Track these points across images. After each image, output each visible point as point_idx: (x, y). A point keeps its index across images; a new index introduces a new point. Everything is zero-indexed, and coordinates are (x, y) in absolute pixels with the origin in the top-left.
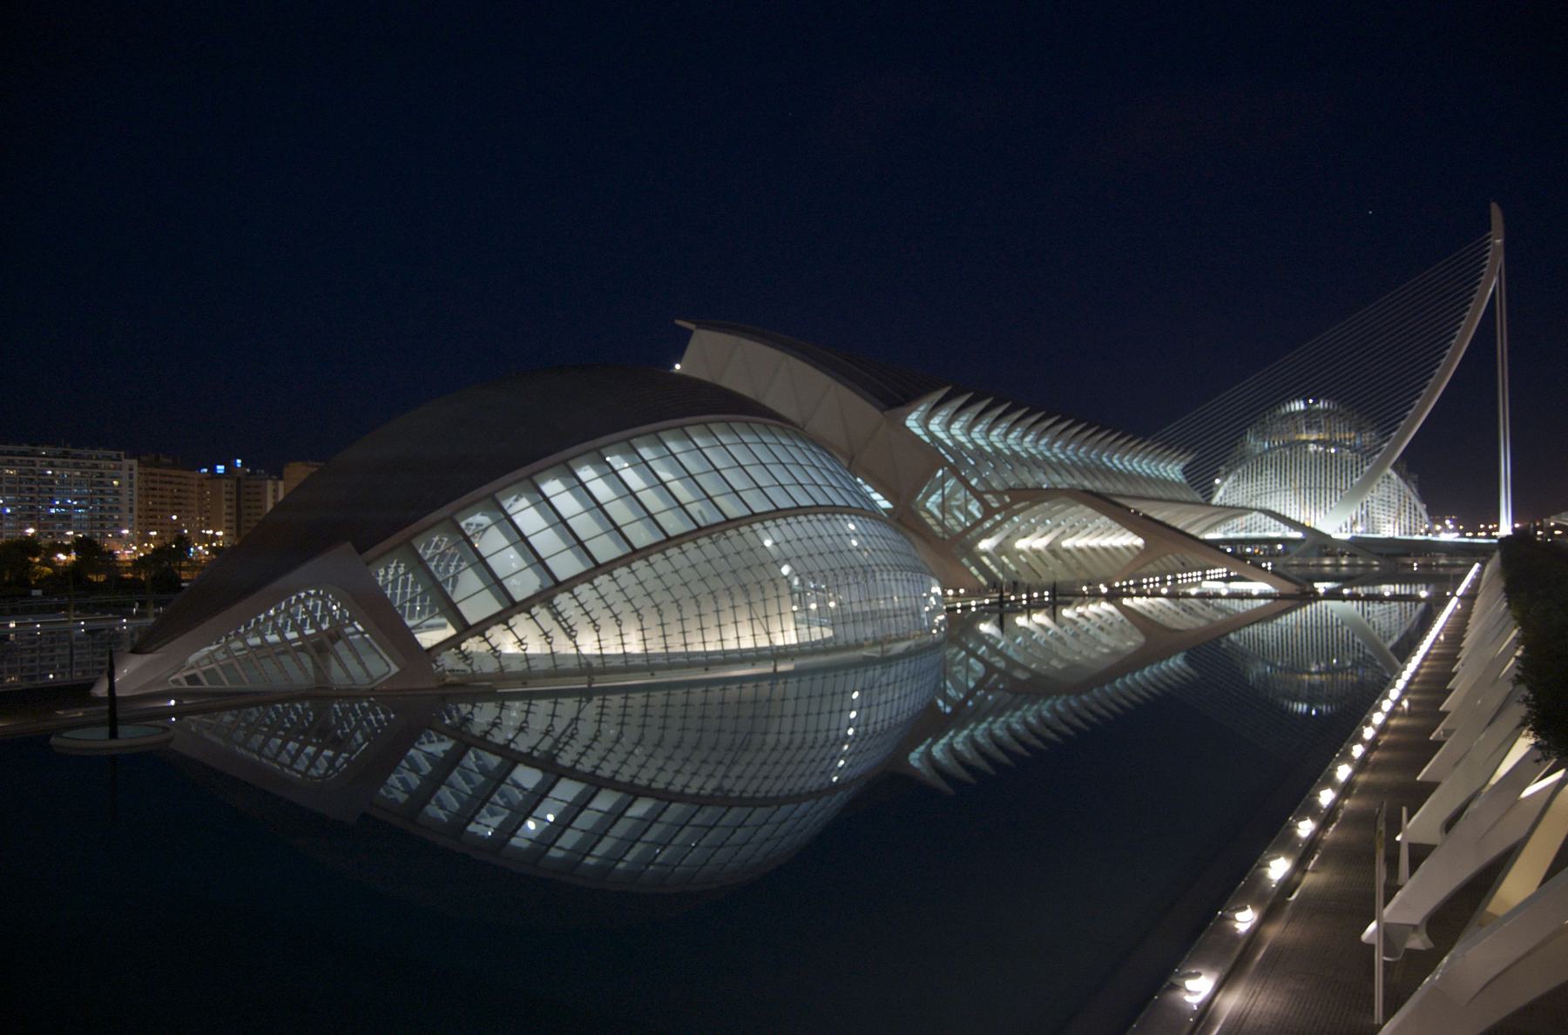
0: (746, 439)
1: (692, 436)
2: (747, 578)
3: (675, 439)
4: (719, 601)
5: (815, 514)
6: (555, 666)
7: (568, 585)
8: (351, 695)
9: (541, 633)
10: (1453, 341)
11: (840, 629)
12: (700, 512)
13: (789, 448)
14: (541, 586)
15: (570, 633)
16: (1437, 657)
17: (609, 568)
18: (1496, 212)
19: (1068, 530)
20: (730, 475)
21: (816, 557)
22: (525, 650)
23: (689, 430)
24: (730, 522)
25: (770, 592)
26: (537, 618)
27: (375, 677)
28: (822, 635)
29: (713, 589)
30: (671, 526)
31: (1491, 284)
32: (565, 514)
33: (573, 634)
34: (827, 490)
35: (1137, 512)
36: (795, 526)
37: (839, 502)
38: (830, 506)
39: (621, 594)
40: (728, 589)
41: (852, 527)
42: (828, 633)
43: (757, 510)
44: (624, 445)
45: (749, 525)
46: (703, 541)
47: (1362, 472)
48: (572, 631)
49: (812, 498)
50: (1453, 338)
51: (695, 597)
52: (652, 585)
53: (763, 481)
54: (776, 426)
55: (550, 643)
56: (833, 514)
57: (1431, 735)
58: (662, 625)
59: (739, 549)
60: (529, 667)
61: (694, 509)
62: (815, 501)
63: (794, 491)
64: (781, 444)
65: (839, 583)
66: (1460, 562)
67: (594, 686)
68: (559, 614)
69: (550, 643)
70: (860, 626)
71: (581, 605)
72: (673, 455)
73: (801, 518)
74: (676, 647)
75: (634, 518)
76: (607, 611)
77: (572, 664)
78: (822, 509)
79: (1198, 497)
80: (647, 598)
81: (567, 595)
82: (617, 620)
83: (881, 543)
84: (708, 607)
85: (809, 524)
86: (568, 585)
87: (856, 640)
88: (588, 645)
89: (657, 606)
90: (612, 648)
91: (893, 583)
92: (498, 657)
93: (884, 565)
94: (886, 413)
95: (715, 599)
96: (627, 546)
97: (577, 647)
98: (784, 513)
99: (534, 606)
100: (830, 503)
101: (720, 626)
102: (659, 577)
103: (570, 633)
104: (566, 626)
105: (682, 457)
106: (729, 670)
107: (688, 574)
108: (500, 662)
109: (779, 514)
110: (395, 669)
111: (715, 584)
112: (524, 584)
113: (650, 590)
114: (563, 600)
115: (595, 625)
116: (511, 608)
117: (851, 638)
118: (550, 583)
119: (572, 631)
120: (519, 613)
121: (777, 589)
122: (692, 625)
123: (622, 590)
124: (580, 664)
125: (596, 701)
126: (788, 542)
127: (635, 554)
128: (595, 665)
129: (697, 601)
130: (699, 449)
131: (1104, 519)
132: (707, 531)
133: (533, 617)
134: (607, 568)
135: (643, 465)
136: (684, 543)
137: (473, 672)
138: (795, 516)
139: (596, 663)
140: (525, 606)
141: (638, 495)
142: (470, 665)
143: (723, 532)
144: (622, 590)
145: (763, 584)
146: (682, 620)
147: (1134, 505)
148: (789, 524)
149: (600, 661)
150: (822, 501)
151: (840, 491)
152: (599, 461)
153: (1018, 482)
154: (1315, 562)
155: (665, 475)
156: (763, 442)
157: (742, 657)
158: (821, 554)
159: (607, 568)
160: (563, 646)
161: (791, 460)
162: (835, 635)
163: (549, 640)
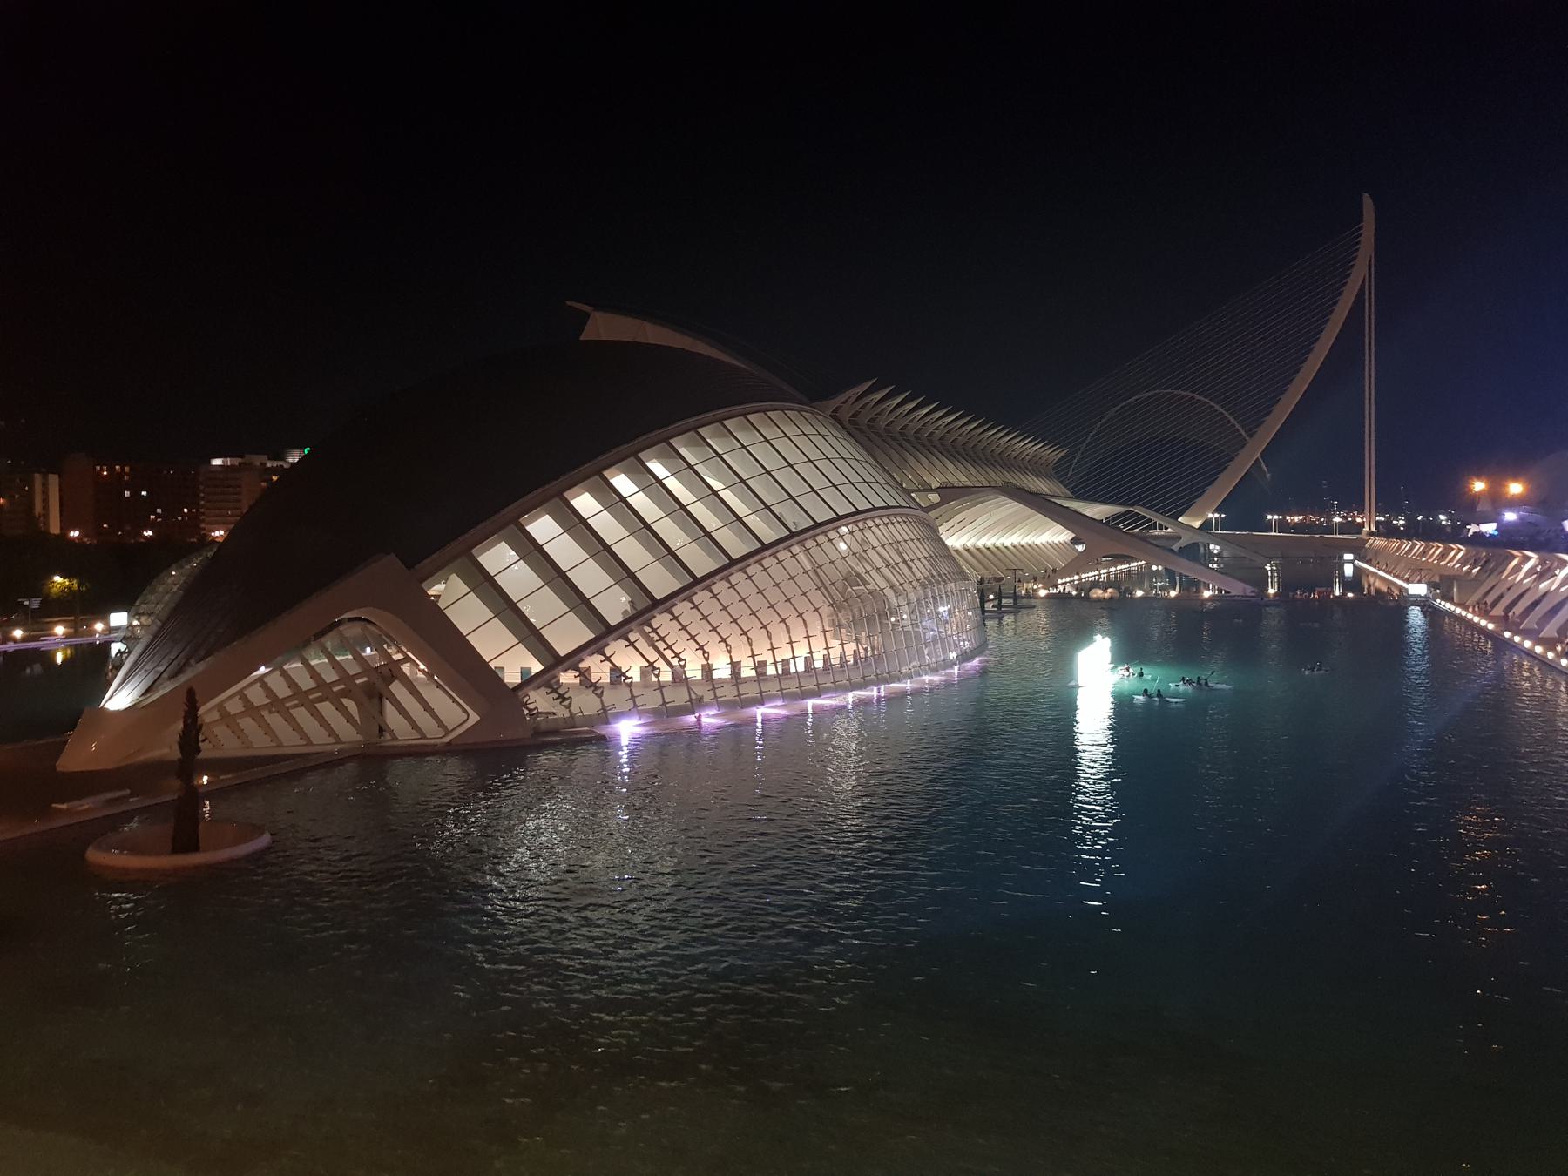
8: (418, 753)
18: (1368, 202)
27: (450, 728)
31: (1361, 272)
61: (753, 521)
63: (808, 501)
78: (844, 521)
110: (474, 718)
112: (614, 604)
114: (661, 621)
115: (704, 652)
116: (604, 633)
118: (644, 603)
135: (688, 472)
137: (572, 715)
142: (568, 707)
155: (716, 485)
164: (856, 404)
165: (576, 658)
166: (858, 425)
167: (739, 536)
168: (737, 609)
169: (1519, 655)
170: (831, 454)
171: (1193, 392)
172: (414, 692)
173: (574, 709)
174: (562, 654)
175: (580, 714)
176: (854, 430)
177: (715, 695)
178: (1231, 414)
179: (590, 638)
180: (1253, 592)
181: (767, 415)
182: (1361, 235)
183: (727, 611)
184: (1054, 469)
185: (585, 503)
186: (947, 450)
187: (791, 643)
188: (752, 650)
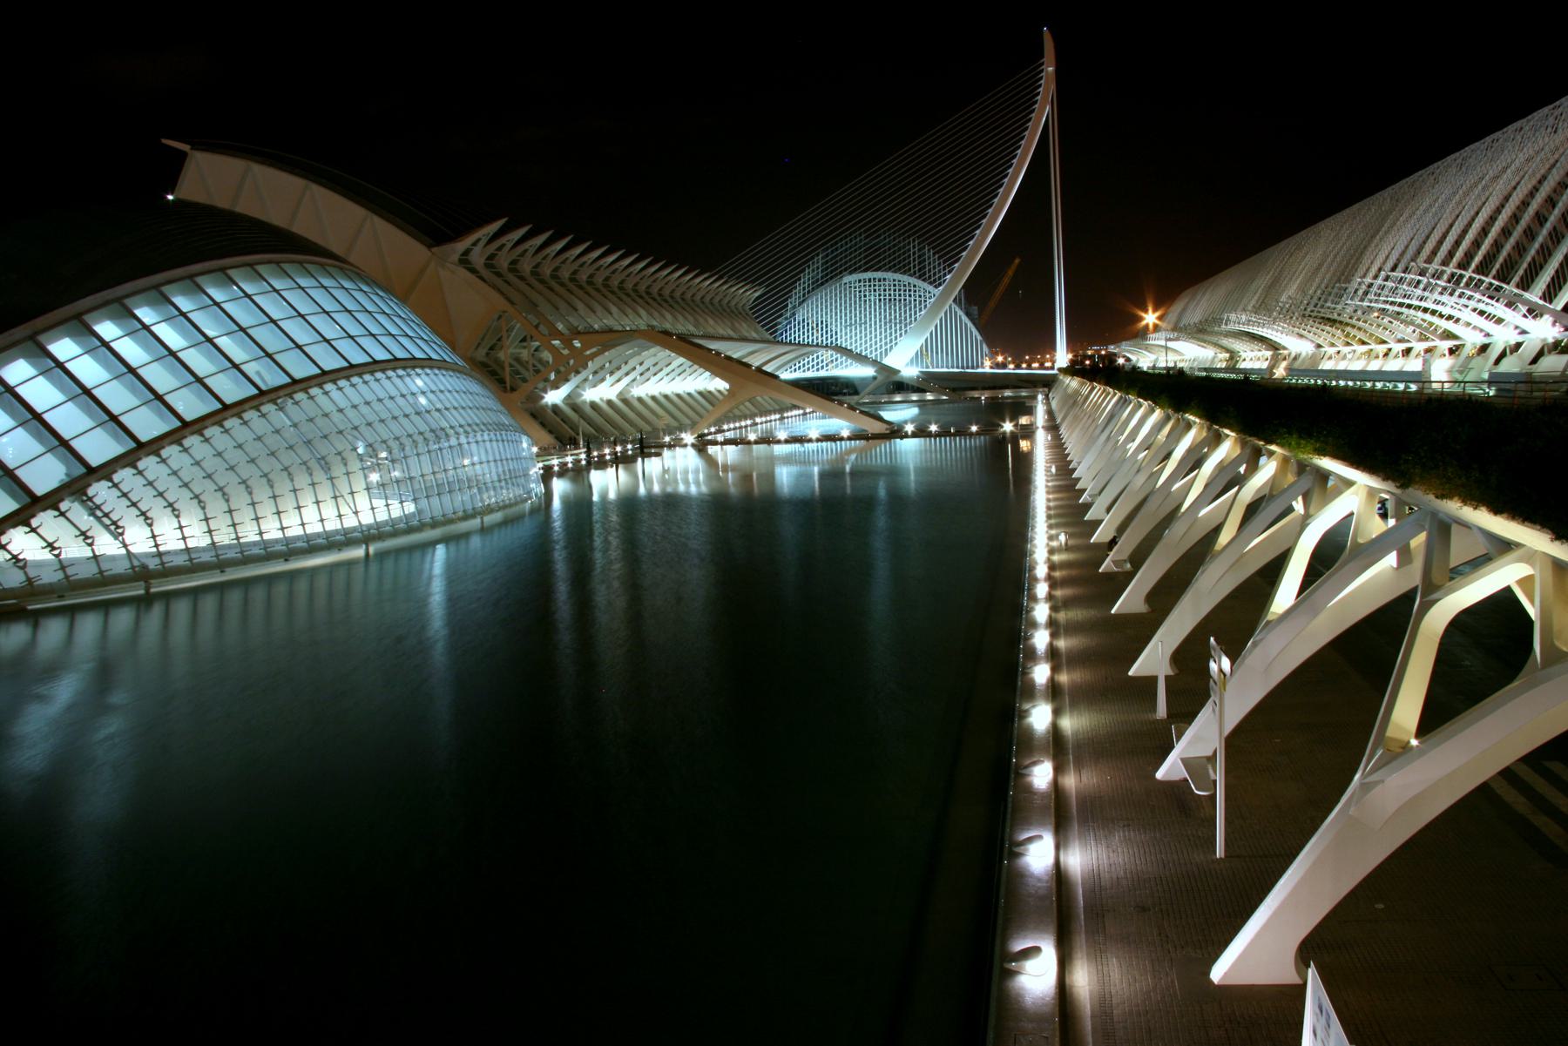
0: (277, 284)
1: (237, 280)
2: (323, 448)
3: (184, 293)
4: (276, 485)
5: (394, 369)
6: (101, 572)
7: (104, 471)
9: (78, 533)
10: (1023, 142)
11: (424, 503)
12: (258, 373)
13: (352, 292)
14: (67, 475)
15: (116, 530)
16: (1057, 489)
17: (155, 447)
19: (638, 377)
20: (293, 327)
21: (402, 420)
22: (57, 556)
23: (232, 273)
24: (297, 384)
25: (338, 470)
26: (67, 514)
28: (404, 512)
29: (286, 465)
30: (181, 408)
31: (1044, 113)
32: (88, 382)
33: (120, 531)
34: (385, 340)
35: (718, 354)
36: (361, 387)
37: (419, 355)
38: (410, 359)
39: (174, 478)
40: (305, 463)
41: (419, 382)
42: (410, 508)
43: (327, 368)
44: (153, 293)
45: (320, 386)
46: (268, 408)
47: (925, 306)
48: (118, 527)
49: (390, 353)
50: (1022, 138)
51: (265, 475)
52: (211, 464)
53: (330, 331)
54: (335, 266)
55: (91, 545)
56: (413, 368)
57: (1099, 568)
58: (230, 511)
59: (312, 415)
60: (67, 577)
62: (393, 355)
63: (367, 342)
64: (343, 287)
65: (420, 451)
66: (1024, 394)
67: (153, 590)
68: (98, 507)
69: (91, 545)
70: (446, 498)
71: (125, 495)
72: (184, 315)
73: (355, 380)
74: (249, 534)
75: (137, 403)
76: (133, 509)
77: (122, 568)
79: (767, 336)
80: (208, 481)
81: (105, 484)
82: (174, 510)
83: (465, 400)
84: (283, 486)
85: (365, 386)
86: (104, 471)
87: (474, 509)
88: (139, 540)
89: (221, 489)
90: (171, 541)
91: (474, 446)
92: (23, 568)
93: (477, 425)
94: (435, 249)
95: (291, 477)
96: (175, 419)
97: (125, 546)
98: (332, 377)
99: (62, 500)
100: (409, 356)
101: (299, 508)
102: (219, 454)
103: (116, 530)
104: (108, 522)
105: (196, 317)
106: (168, 583)
107: (254, 449)
108: (26, 573)
109: (326, 378)
111: (287, 458)
113: (186, 480)
114: (100, 491)
117: (438, 513)
119: (118, 527)
120: (44, 510)
121: (346, 465)
122: (266, 509)
123: (175, 473)
124: (133, 567)
125: (157, 610)
126: (355, 407)
127: (185, 428)
128: (152, 566)
129: (289, 474)
130: (217, 304)
131: (681, 360)
132: (235, 410)
133: (62, 514)
134: (153, 447)
136: (244, 411)
138: (348, 378)
139: (153, 564)
140: (51, 501)
141: (180, 355)
143: (290, 395)
144: (175, 473)
145: (344, 454)
146: (253, 504)
147: (714, 345)
148: (353, 386)
149: (157, 561)
150: (400, 354)
151: (418, 341)
152: (125, 314)
153: (586, 325)
154: (886, 400)
156: (300, 287)
157: (312, 545)
158: (382, 421)
159: (153, 447)
160: (106, 545)
161: (338, 307)
162: (419, 511)
163: (89, 541)
166: (560, 279)
168: (148, 501)
170: (329, 305)
179: (130, 447)
180: (887, 429)
185: (64, 348)
186: (666, 301)
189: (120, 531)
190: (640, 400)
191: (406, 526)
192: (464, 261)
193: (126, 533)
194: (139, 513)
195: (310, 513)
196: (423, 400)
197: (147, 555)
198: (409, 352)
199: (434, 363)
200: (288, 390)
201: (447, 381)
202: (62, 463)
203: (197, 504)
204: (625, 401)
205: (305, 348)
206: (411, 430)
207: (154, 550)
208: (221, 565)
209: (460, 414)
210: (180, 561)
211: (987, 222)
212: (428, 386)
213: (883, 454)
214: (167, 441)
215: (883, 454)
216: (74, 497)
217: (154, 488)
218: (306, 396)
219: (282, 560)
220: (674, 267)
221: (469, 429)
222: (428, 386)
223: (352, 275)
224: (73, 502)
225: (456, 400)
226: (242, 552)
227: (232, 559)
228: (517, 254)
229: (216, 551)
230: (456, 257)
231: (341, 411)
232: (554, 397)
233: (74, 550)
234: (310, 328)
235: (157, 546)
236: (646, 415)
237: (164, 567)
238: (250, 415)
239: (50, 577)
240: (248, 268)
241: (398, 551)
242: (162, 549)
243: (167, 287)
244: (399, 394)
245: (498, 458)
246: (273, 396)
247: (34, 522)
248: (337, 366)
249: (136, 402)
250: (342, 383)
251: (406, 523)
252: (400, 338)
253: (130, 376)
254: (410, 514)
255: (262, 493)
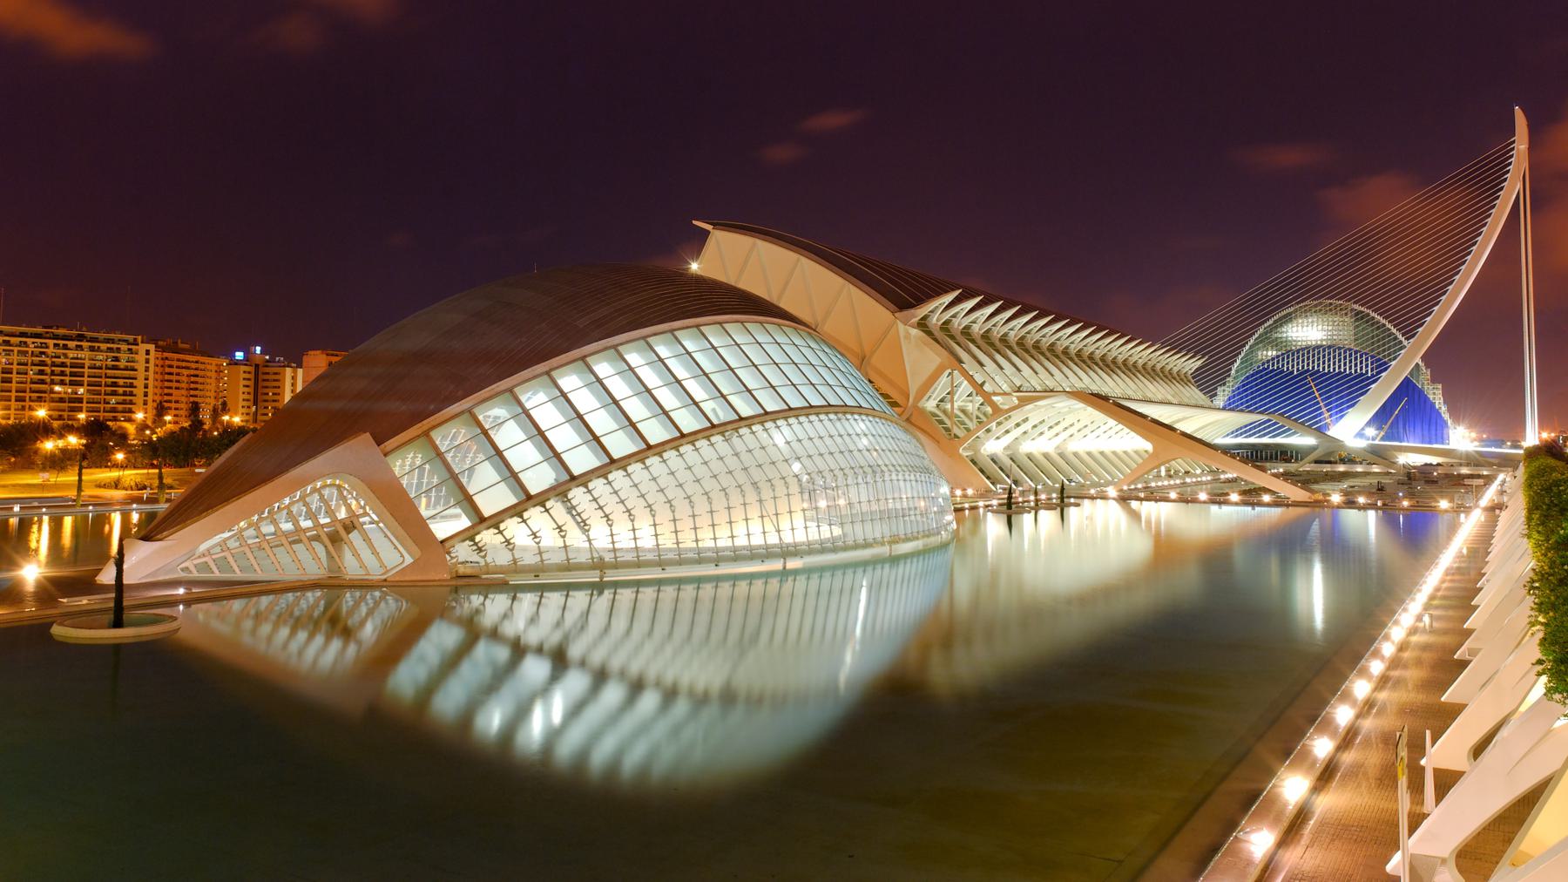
3: (665, 344)
7: (582, 480)
8: (364, 586)
11: (848, 528)
14: (555, 480)
21: (827, 456)
28: (832, 533)
34: (822, 389)
37: (850, 402)
38: (843, 406)
41: (862, 425)
42: (837, 531)
46: (717, 439)
48: (586, 525)
55: (564, 537)
56: (845, 413)
60: (542, 561)
63: (806, 390)
68: (574, 508)
69: (564, 537)
77: (583, 558)
83: (887, 444)
86: (582, 480)
88: (601, 537)
97: (589, 540)
98: (773, 416)
99: (548, 499)
103: (583, 526)
104: (580, 520)
108: (513, 555)
110: (409, 560)
119: (586, 525)
124: (592, 558)
125: (608, 594)
132: (690, 439)
139: (608, 557)
140: (540, 500)
142: (484, 557)
149: (612, 555)
151: (866, 396)
160: (575, 538)
162: (845, 535)
164: (987, 323)
165: (499, 518)
167: (665, 427)
169: (38, 520)
171: (1369, 308)
172: (367, 540)
173: (489, 559)
174: (486, 513)
175: (493, 564)
176: (985, 345)
177: (541, 556)
178: (1399, 330)
181: (764, 327)
182: (1513, 149)
183: (638, 488)
184: (1193, 378)
187: (747, 520)
188: (654, 520)
189: (587, 528)
190: (1030, 457)
191: (832, 546)
192: (923, 325)
193: (591, 530)
194: (625, 510)
195: (723, 532)
196: (865, 441)
197: (604, 550)
198: (806, 400)
199: (875, 413)
200: (735, 426)
201: (882, 428)
202: (553, 470)
203: (649, 512)
204: (1062, 455)
205: (777, 388)
206: (863, 463)
207: (611, 546)
208: (661, 564)
209: (893, 456)
210: (629, 557)
211: (1438, 309)
212: (869, 430)
213: (906, 578)
214: (633, 459)
215: (906, 578)
216: (557, 498)
217: (597, 503)
218: (750, 431)
219: (660, 568)
220: (1138, 341)
221: (899, 469)
222: (869, 430)
223: (818, 339)
224: (557, 502)
225: (891, 444)
226: (679, 555)
227: (628, 561)
228: (970, 321)
229: (638, 553)
230: (915, 320)
231: (811, 439)
232: (993, 446)
233: (550, 539)
234: (761, 376)
235: (613, 543)
236: (1089, 463)
237: (660, 559)
238: (702, 443)
239: (530, 559)
240: (718, 326)
241: (821, 569)
242: (617, 546)
243: (652, 338)
244: (827, 435)
245: (921, 495)
246: (721, 429)
247: (526, 515)
248: (776, 408)
249: (616, 427)
250: (802, 419)
251: (833, 543)
252: (851, 391)
253: (614, 406)
254: (825, 539)
255: (719, 503)
